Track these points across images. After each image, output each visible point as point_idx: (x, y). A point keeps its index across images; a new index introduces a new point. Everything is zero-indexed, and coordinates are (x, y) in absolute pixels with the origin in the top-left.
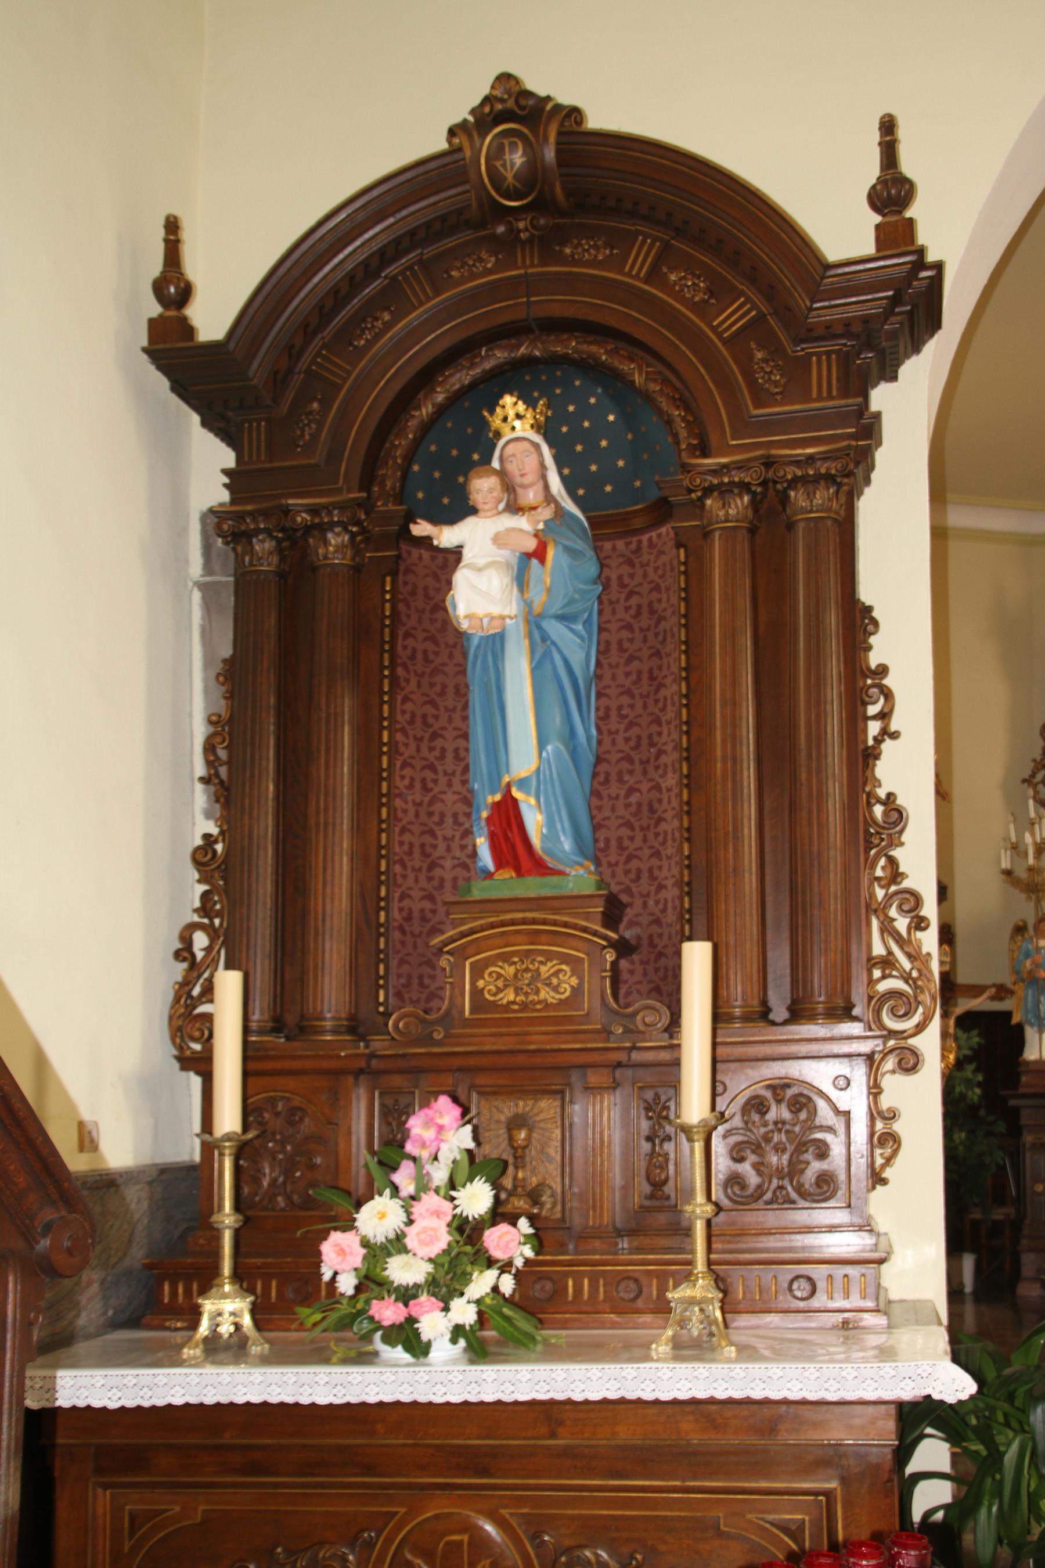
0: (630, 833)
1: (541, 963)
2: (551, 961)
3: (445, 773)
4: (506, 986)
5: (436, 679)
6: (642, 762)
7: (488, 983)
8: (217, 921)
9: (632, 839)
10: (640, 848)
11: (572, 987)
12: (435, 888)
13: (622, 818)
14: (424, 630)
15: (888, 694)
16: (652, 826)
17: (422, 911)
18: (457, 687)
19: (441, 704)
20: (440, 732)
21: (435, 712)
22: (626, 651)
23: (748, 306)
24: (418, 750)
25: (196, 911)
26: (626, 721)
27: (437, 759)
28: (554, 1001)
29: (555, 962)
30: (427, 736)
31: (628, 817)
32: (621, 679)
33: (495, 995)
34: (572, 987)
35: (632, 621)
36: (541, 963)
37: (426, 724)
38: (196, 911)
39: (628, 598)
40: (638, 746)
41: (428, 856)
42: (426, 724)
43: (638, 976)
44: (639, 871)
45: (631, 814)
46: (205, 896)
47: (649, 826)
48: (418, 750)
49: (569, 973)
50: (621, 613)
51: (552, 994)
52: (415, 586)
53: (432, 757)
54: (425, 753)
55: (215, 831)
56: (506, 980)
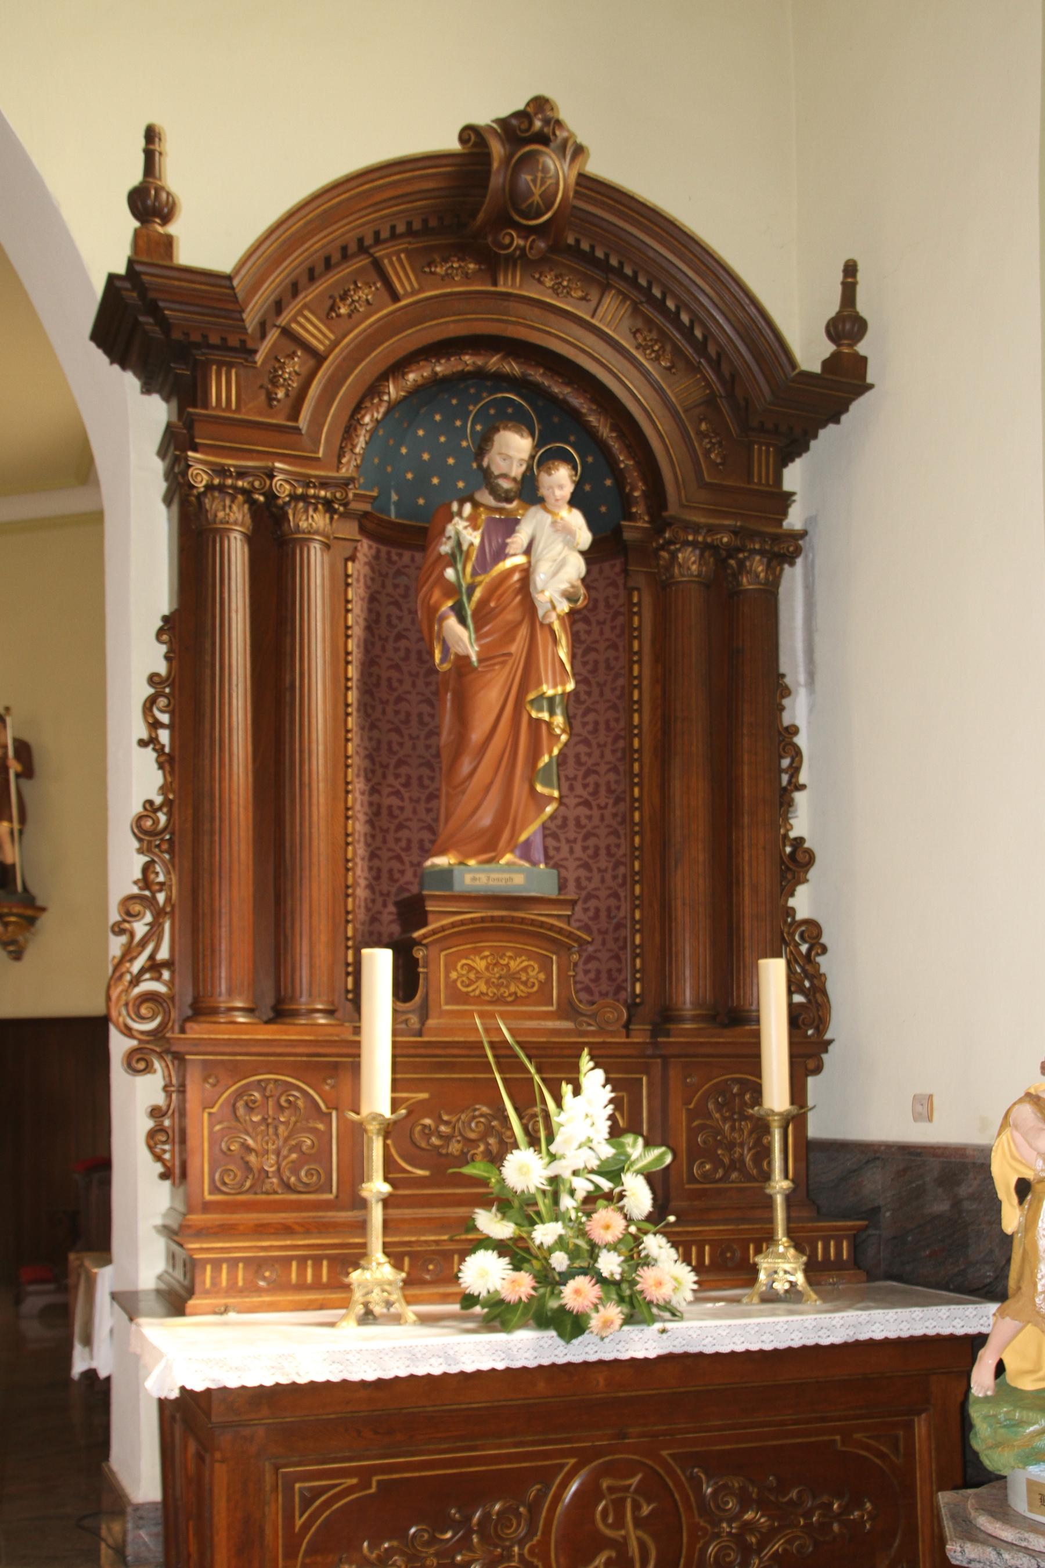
0: (587, 750)
1: (510, 958)
2: (520, 956)
3: (411, 737)
4: (478, 978)
5: (400, 834)
6: (598, 684)
7: (460, 976)
8: (161, 897)
9: (589, 879)
10: (597, 642)
11: (540, 982)
12: (403, 849)
13: (581, 797)
14: (388, 595)
15: (797, 753)
16: (610, 806)
17: (390, 807)
18: (419, 653)
19: (406, 859)
20: (404, 633)
21: (401, 867)
22: (584, 827)
23: (694, 1249)
24: (384, 841)
25: (136, 883)
26: (584, 707)
27: (403, 849)
28: (523, 995)
29: (523, 958)
30: (393, 827)
31: (586, 920)
32: (580, 977)
33: (468, 986)
34: (540, 982)
35: (590, 798)
36: (510, 958)
37: (391, 688)
38: (136, 883)
39: (584, 715)
40: (596, 855)
41: (396, 881)
42: (391, 688)
43: (596, 821)
44: (597, 848)
45: (589, 857)
46: (146, 869)
47: (607, 804)
48: (384, 841)
49: (537, 969)
50: (579, 790)
51: (522, 987)
52: (379, 677)
53: (397, 784)
54: (391, 843)
55: (158, 800)
56: (477, 972)
